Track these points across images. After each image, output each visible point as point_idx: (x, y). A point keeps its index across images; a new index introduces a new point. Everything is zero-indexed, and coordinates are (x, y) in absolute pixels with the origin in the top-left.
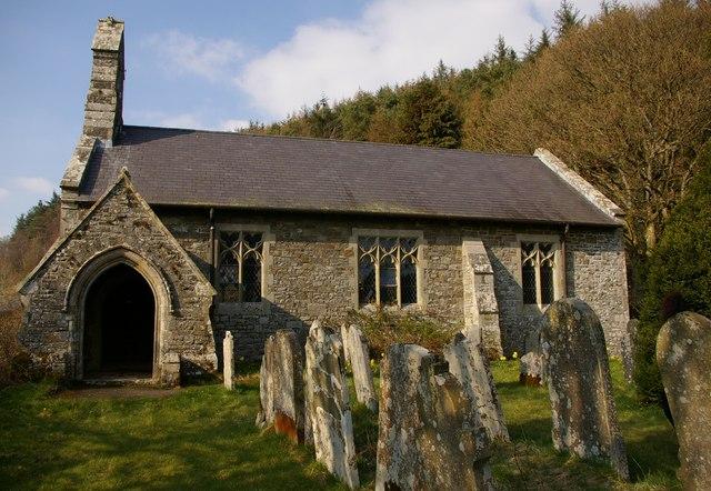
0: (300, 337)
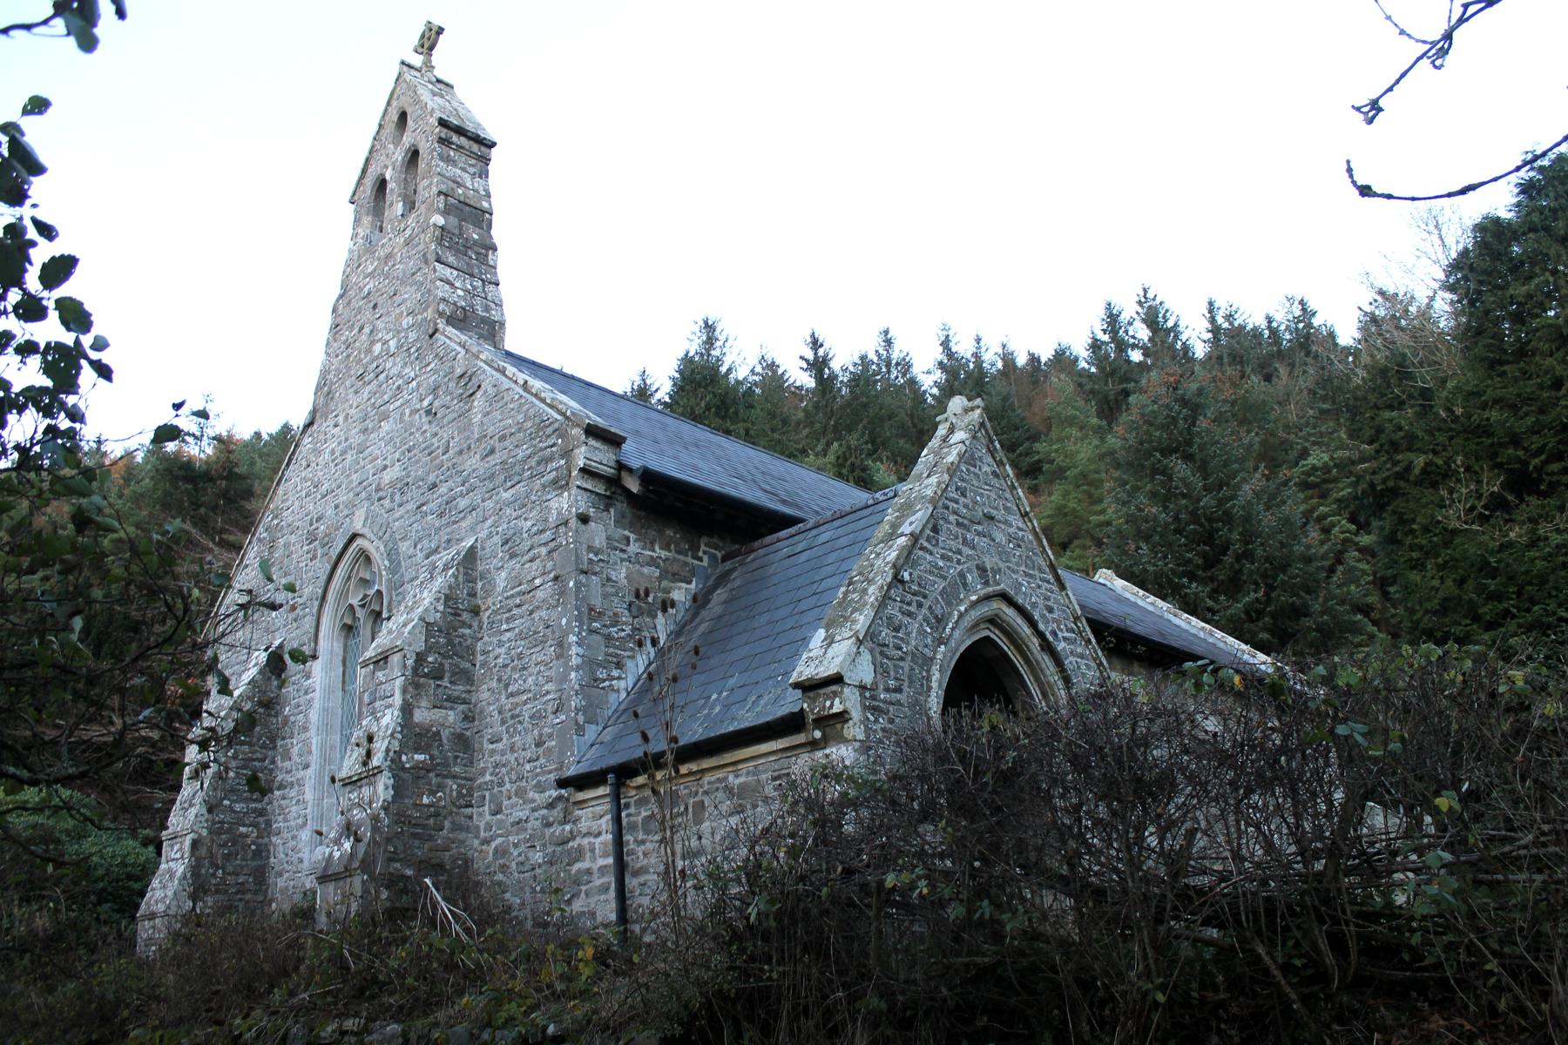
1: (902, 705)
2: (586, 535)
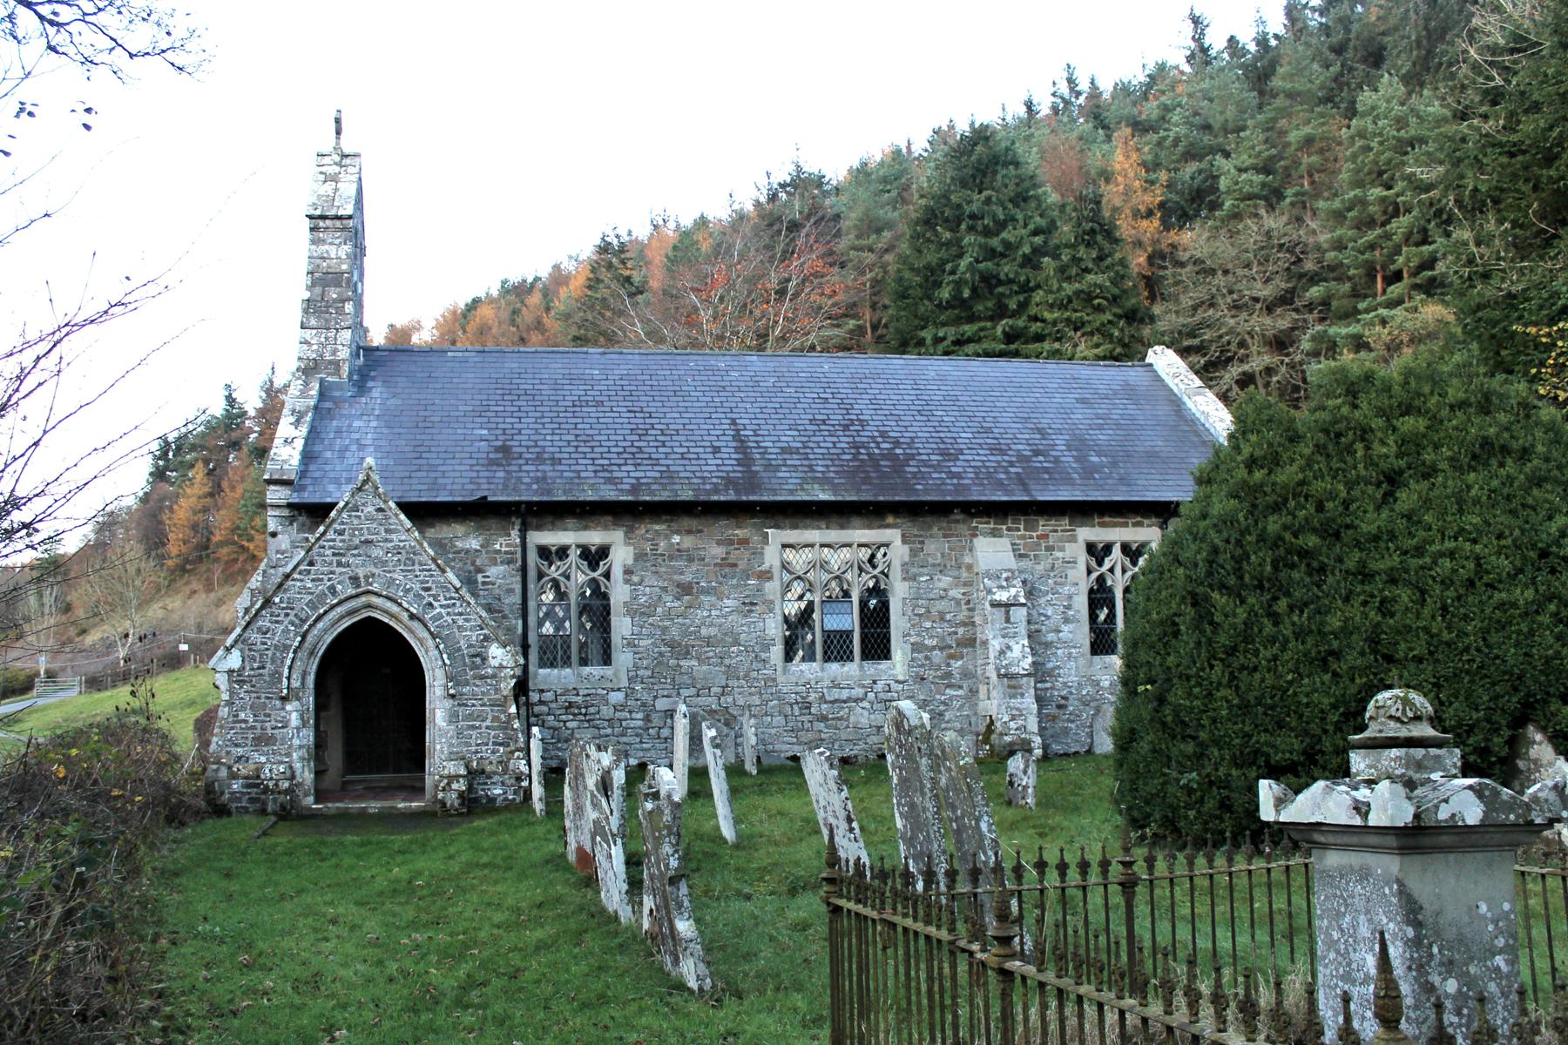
0: (1264, 973)
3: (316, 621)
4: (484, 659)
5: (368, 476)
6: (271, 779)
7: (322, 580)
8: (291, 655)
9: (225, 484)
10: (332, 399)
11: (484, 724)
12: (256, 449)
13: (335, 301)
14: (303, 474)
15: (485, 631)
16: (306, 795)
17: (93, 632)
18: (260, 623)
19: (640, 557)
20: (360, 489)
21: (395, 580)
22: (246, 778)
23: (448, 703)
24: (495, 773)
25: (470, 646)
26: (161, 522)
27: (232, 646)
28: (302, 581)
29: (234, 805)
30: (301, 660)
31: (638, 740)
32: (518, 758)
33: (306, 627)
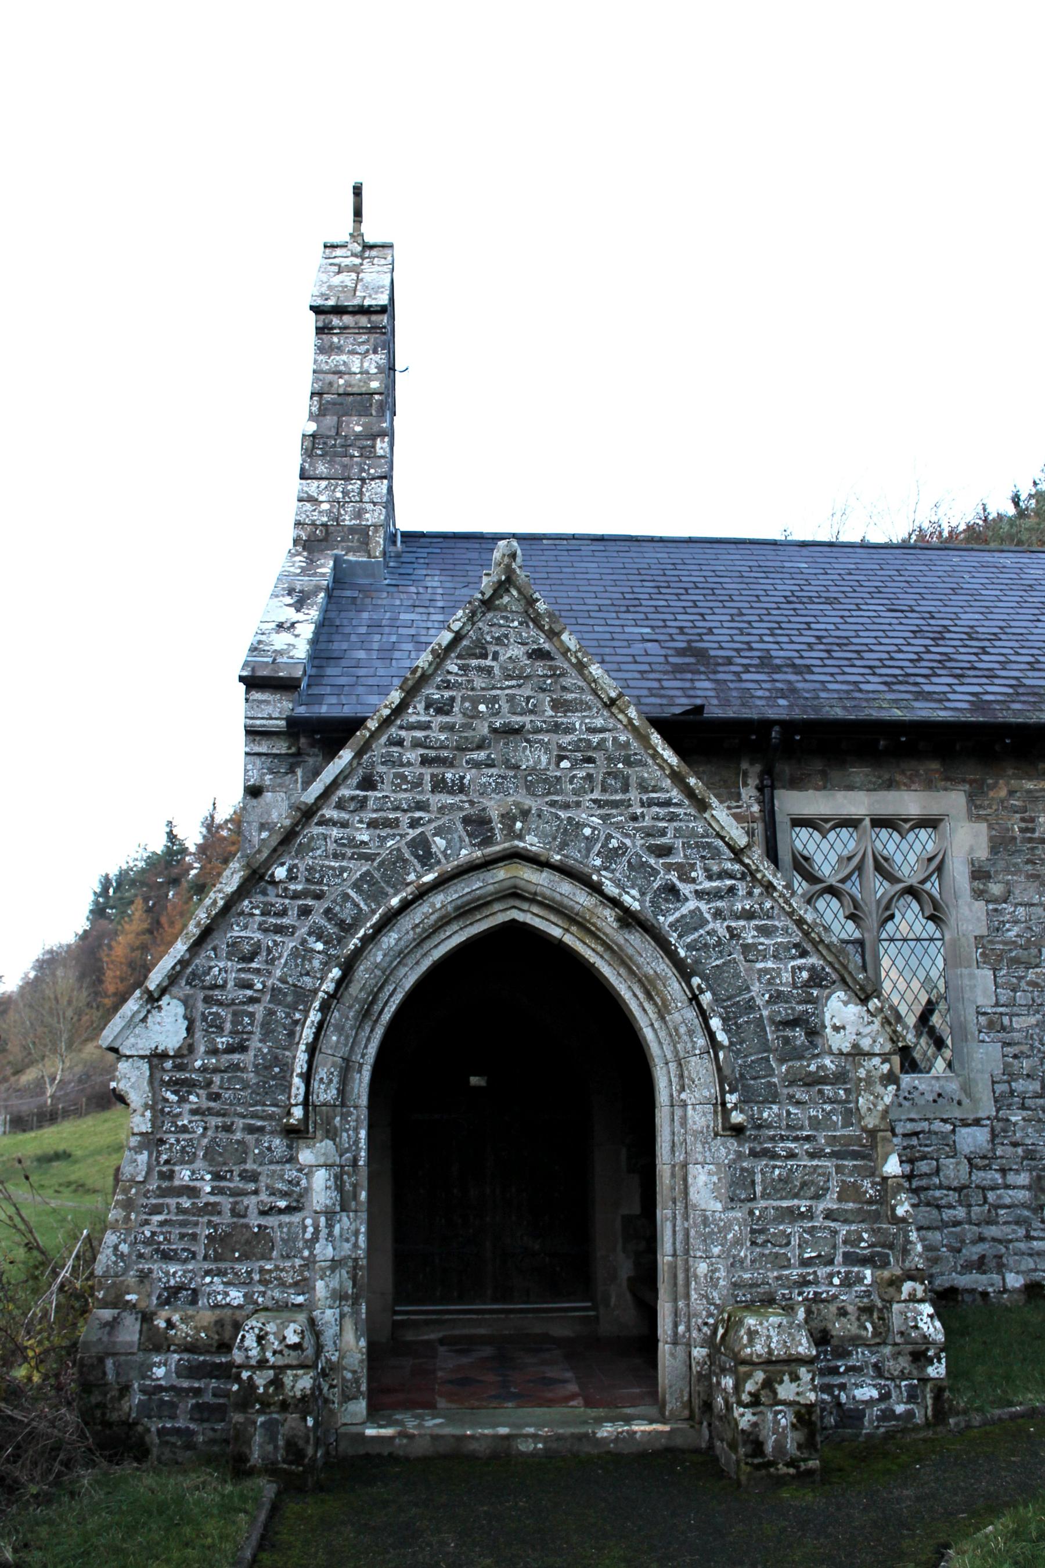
1: (243, 1070)
2: (259, 811)
3: (380, 929)
4: (814, 1033)
5: (509, 571)
6: (262, 1364)
7: (395, 824)
8: (314, 1016)
9: (164, 920)
10: (353, 586)
11: (821, 1206)
12: (197, 885)
13: (358, 436)
14: (315, 680)
15: (813, 960)
16: (347, 1398)
17: (28, 1071)
18: (236, 932)
19: (1000, 844)
20: (488, 604)
21: (580, 826)
22: (191, 1348)
23: (726, 1149)
24: (857, 1341)
25: (777, 997)
26: (100, 960)
27: (163, 991)
28: (344, 825)
29: (155, 1425)
30: (340, 1029)
31: (1021, 1232)
32: (913, 1299)
33: (354, 942)
